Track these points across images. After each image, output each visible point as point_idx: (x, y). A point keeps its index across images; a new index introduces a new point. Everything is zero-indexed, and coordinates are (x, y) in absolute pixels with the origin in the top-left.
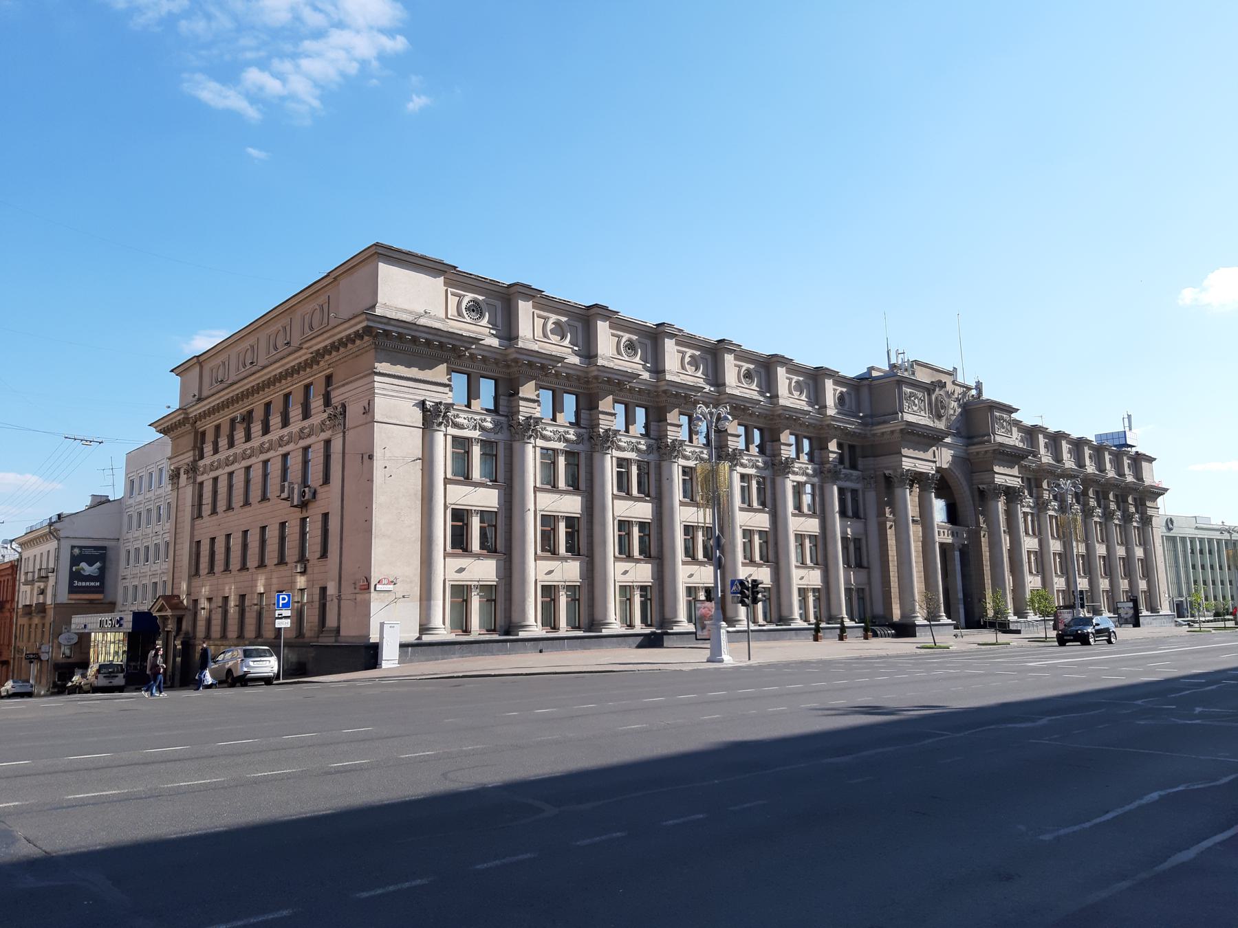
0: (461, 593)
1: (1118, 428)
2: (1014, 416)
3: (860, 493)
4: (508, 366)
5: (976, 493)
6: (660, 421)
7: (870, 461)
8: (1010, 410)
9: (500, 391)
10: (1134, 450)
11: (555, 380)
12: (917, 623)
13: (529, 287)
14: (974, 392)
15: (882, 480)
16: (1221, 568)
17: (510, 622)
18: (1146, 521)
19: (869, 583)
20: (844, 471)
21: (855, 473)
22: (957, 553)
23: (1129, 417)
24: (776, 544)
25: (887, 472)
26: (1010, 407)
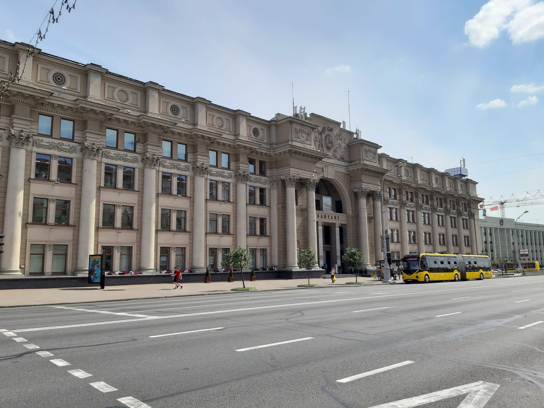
0: (213, 252)
1: (457, 165)
2: (379, 151)
3: (267, 190)
4: (193, 138)
5: (353, 194)
6: (194, 153)
7: (275, 171)
8: (378, 147)
9: (188, 151)
10: (466, 177)
11: (171, 135)
12: (368, 268)
13: (205, 99)
14: (355, 136)
15: (280, 182)
16: (540, 244)
17: (140, 267)
18: (472, 216)
19: (271, 246)
20: (409, 203)
21: (263, 178)
22: (337, 230)
23: (464, 160)
24: (192, 219)
25: (282, 178)
26: (377, 145)
